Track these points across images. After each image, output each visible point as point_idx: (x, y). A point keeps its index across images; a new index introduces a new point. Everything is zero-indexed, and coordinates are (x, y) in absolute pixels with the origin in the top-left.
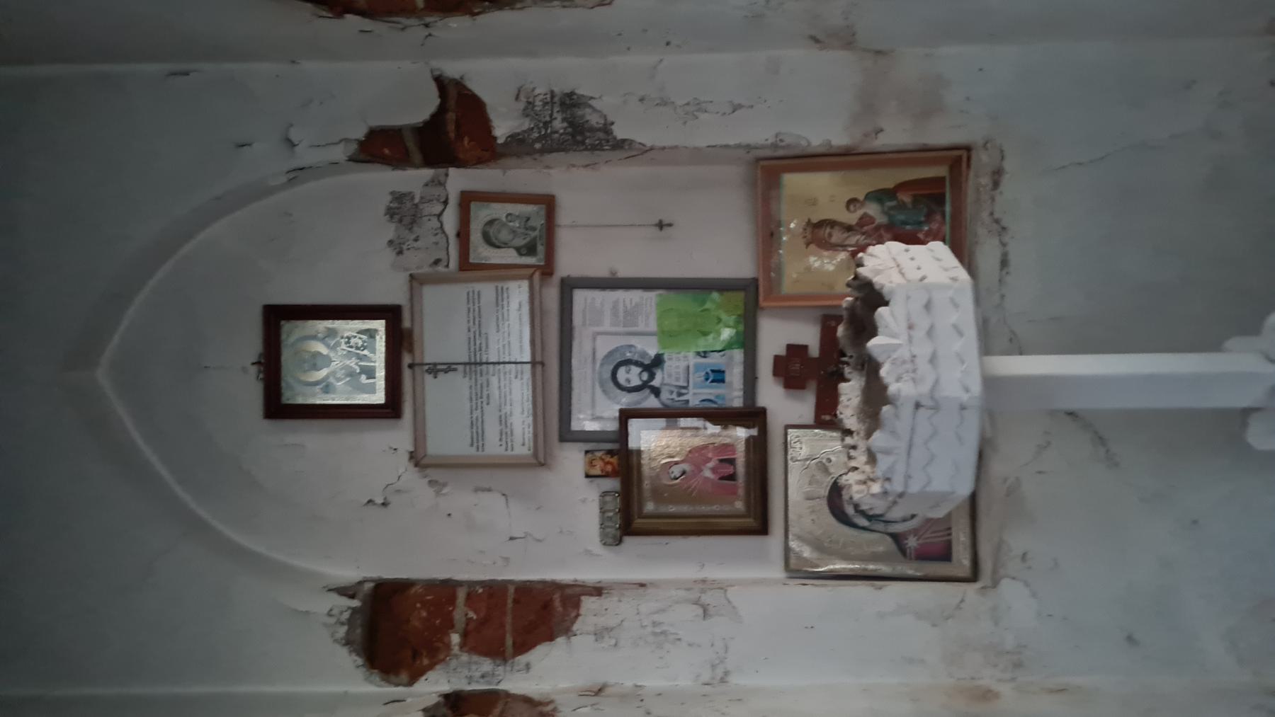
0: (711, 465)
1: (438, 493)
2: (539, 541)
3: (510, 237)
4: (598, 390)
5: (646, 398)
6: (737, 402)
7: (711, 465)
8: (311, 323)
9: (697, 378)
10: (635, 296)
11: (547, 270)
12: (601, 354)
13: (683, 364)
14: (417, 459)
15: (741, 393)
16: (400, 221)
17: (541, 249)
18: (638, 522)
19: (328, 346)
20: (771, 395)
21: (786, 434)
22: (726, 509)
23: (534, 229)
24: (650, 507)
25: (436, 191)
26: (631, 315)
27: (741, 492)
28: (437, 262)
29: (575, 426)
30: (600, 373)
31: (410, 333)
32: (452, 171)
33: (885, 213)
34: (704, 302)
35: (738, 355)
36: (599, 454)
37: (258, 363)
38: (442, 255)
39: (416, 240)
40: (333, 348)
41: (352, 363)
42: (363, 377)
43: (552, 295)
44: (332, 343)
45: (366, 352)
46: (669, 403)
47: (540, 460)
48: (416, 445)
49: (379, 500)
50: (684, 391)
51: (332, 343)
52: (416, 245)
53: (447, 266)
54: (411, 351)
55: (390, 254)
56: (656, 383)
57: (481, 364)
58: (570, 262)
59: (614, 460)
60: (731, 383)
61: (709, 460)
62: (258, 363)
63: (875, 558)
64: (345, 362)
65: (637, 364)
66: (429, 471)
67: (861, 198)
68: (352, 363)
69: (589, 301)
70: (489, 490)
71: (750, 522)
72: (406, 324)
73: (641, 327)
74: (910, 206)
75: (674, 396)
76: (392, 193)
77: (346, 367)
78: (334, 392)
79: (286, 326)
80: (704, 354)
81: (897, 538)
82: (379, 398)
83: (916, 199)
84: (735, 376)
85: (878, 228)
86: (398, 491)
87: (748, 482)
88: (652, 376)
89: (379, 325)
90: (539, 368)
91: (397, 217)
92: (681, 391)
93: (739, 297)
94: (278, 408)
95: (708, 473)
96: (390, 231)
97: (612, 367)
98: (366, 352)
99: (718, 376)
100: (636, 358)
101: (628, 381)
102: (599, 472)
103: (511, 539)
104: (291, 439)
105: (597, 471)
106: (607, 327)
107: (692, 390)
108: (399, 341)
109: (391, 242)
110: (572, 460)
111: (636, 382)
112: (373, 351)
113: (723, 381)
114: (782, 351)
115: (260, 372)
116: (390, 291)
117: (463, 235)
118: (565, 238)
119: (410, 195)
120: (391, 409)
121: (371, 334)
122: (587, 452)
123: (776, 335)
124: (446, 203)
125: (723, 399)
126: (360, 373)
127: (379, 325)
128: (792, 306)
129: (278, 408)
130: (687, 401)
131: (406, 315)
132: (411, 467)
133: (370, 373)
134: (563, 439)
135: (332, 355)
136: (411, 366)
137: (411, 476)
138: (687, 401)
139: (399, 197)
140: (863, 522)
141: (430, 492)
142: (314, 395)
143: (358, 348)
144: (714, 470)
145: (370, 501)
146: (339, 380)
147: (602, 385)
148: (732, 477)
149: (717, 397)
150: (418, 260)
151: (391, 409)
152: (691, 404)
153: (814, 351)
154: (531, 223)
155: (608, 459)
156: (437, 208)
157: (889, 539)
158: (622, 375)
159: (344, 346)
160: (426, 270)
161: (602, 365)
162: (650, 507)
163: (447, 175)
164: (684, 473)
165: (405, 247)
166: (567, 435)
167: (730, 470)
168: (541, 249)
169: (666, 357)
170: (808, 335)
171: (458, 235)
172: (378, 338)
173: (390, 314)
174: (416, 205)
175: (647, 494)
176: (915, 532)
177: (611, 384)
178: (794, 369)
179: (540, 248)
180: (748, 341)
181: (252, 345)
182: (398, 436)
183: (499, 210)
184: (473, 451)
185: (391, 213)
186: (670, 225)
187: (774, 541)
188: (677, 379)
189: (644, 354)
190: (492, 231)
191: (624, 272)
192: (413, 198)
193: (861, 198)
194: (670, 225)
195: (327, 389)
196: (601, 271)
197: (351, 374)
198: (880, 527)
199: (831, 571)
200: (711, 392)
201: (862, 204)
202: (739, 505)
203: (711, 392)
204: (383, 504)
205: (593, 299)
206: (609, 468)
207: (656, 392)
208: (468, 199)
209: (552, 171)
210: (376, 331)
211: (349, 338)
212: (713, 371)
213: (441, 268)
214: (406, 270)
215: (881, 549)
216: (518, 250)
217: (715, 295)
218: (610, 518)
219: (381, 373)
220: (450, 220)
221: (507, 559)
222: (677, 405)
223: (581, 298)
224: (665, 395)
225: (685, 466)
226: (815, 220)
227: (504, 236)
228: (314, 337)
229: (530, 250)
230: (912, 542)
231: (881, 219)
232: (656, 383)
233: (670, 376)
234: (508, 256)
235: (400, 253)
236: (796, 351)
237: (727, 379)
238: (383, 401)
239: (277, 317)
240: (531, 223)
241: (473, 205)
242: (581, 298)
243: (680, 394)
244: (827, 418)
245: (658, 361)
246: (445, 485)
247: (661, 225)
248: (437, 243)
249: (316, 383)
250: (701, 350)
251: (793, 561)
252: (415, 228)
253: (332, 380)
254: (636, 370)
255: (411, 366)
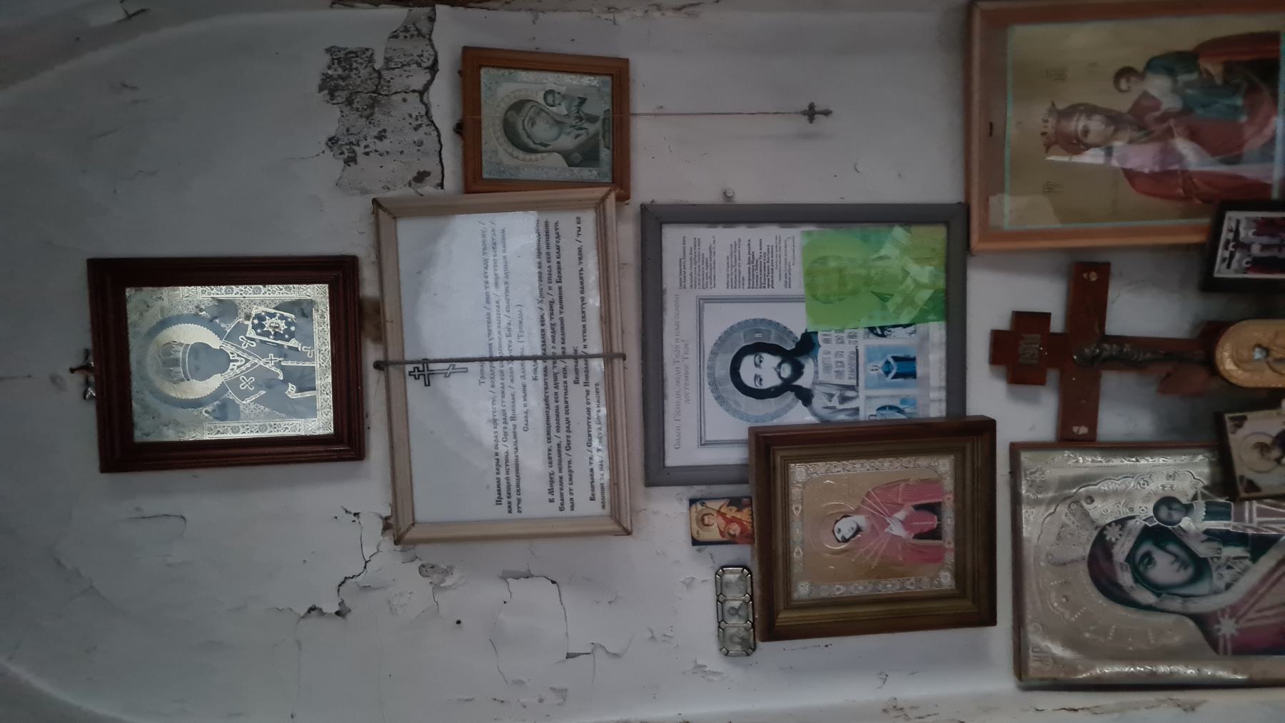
0: (901, 515)
1: (436, 587)
2: (615, 655)
3: (554, 132)
4: (709, 396)
5: (790, 407)
6: (934, 408)
7: (901, 515)
8: (166, 292)
9: (871, 371)
10: (768, 235)
11: (620, 180)
12: (710, 339)
13: (848, 348)
14: (397, 528)
15: (943, 395)
16: (349, 102)
17: (605, 154)
18: (784, 617)
19: (220, 333)
20: (988, 395)
21: (382, 290)
22: (926, 586)
23: (592, 119)
24: (803, 590)
25: (415, 47)
26: (760, 270)
27: (950, 558)
28: (421, 177)
29: (674, 458)
30: (711, 368)
31: (378, 307)
32: (441, 9)
33: (1175, 91)
34: (880, 245)
35: (936, 331)
36: (715, 505)
37: (85, 368)
38: (431, 165)
39: (381, 137)
40: (231, 337)
41: (270, 363)
42: (291, 388)
43: (626, 235)
44: (229, 328)
45: (293, 343)
46: (825, 413)
47: (621, 523)
48: (394, 507)
49: (331, 607)
50: (850, 394)
51: (229, 328)
52: (381, 146)
53: (441, 185)
54: (380, 338)
55: (333, 165)
56: (804, 381)
57: (544, 358)
58: (653, 180)
59: (744, 515)
60: (927, 378)
61: (899, 507)
62: (85, 368)
63: (1170, 655)
64: (235, 358)
65: (774, 350)
66: (420, 549)
67: (1140, 67)
68: (270, 363)
69: (690, 244)
70: (528, 576)
71: (965, 605)
72: (369, 289)
73: (779, 289)
74: (1219, 81)
75: (835, 402)
76: (329, 50)
77: (259, 372)
78: (237, 418)
79: (135, 297)
80: (882, 332)
81: (1202, 621)
82: (320, 423)
83: (1229, 69)
84: (933, 365)
85: (1164, 118)
86: (366, 588)
87: (960, 541)
88: (798, 371)
89: (317, 293)
90: (617, 363)
91: (341, 96)
92: (846, 392)
93: (936, 236)
94: (126, 448)
95: (897, 530)
96: (330, 119)
97: (731, 356)
98: (293, 343)
99: (904, 368)
100: (773, 340)
101: (758, 378)
102: (717, 537)
103: (569, 656)
104: (152, 505)
105: (713, 534)
106: (721, 289)
107: (863, 392)
108: (357, 321)
109: (333, 141)
110: (668, 514)
111: (771, 381)
112: (308, 339)
113: (913, 375)
114: (1004, 324)
115: (87, 383)
116: (337, 229)
117: (468, 129)
118: (645, 134)
119: (365, 54)
120: (346, 442)
121: (303, 309)
122: (692, 502)
123: (995, 298)
124: (433, 69)
125: (914, 404)
126: (285, 382)
127: (317, 293)
128: (1017, 251)
129: (126, 448)
130: (857, 410)
131: (368, 275)
132: (387, 543)
133: (305, 381)
134: (650, 482)
135: (229, 349)
136: (378, 366)
137: (386, 557)
138: (857, 410)
139: (344, 59)
140: (1147, 597)
141: (422, 586)
142: (199, 424)
143: (277, 336)
144: (905, 523)
145: (312, 609)
146: (244, 395)
147: (714, 384)
148: (935, 534)
149: (904, 401)
150: (386, 173)
151: (346, 442)
152: (863, 416)
153: (1057, 325)
154: (588, 109)
155: (732, 512)
156: (419, 79)
157: (1191, 624)
158: (747, 365)
159: (251, 333)
160: (401, 191)
161: (714, 354)
162: (803, 590)
163: (432, 19)
164: (858, 530)
165: (360, 150)
166: (657, 473)
167: (930, 522)
168: (605, 154)
169: (820, 338)
170: (1046, 296)
171: (459, 129)
172: (316, 316)
173: (337, 272)
174: (379, 72)
175: (797, 569)
176: (1233, 611)
177: (730, 386)
178: (1022, 352)
179: (605, 152)
180: (952, 305)
181: (74, 335)
182: (363, 489)
183: (531, 84)
184: (501, 512)
185: (329, 87)
186: (827, 113)
187: (999, 636)
188: (839, 374)
189: (785, 331)
190: (520, 123)
191: (747, 194)
192: (371, 60)
193: (1140, 67)
194: (827, 113)
195: (224, 410)
196: (706, 194)
197: (268, 383)
198: (1176, 604)
199: (1099, 677)
200: (892, 393)
201: (1141, 76)
202: (946, 580)
203: (892, 393)
204: (338, 613)
205: (697, 242)
206: (735, 529)
207: (805, 397)
208: (474, 62)
209: (619, 18)
210: (312, 303)
211: (260, 318)
212: (895, 359)
213: (428, 189)
214: (364, 192)
215: (1177, 640)
216: (566, 155)
217: (898, 232)
218: (735, 612)
219: (324, 381)
220: (443, 101)
221: (562, 693)
222: (842, 417)
223: (674, 238)
224: (819, 402)
225: (861, 520)
226: (1061, 106)
227: (542, 130)
228: (180, 319)
229: (587, 156)
230: (1227, 628)
231: (1170, 103)
232: (804, 381)
233: (827, 368)
234: (552, 166)
235: (351, 160)
236: (1028, 322)
237: (920, 371)
238: (330, 430)
239: (115, 283)
240: (588, 109)
241: (486, 75)
242: (674, 238)
243: (844, 399)
244: (1083, 430)
245: (808, 344)
246: (447, 572)
247: (811, 113)
248: (421, 144)
249: (197, 403)
250: (877, 323)
251: (1033, 664)
252: (378, 115)
253: (231, 395)
254: (770, 361)
255: (378, 366)
